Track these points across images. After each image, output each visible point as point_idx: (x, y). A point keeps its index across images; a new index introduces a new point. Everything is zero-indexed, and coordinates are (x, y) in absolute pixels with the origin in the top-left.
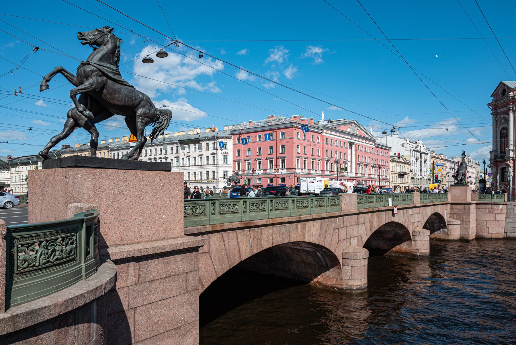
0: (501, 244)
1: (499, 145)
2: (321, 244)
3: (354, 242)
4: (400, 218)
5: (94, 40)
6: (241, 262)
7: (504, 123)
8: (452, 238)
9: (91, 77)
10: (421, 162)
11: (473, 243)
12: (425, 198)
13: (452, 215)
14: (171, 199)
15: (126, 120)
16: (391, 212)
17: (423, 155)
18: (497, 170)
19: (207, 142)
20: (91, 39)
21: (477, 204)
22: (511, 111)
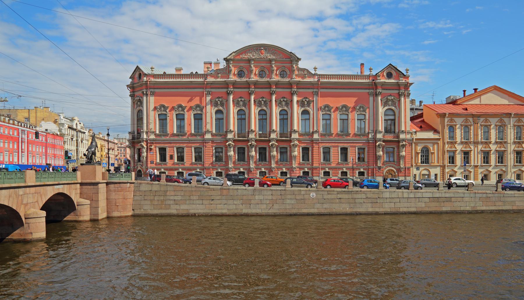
1: (136, 126)
7: (139, 106)
8: (81, 219)
10: (77, 140)
12: (44, 176)
13: (82, 195)
17: (80, 134)
18: (134, 151)
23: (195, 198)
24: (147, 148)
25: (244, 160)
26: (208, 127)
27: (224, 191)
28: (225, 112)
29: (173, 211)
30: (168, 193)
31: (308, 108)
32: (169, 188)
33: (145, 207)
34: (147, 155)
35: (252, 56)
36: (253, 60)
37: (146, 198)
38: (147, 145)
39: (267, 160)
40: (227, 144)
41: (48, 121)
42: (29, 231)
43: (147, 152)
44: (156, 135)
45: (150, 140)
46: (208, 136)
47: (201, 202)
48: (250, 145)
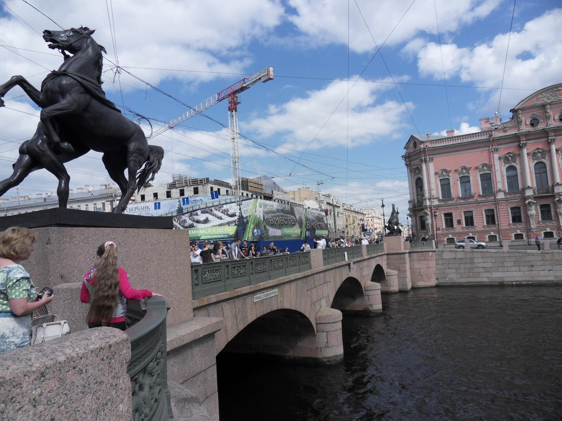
0: (434, 290)
2: (298, 310)
3: (323, 302)
4: (354, 273)
5: (69, 43)
6: (228, 343)
7: (418, 174)
9: (70, 94)
10: (334, 214)
11: (411, 293)
14: (177, 268)
15: (105, 160)
16: (348, 267)
18: (416, 219)
19: (104, 201)
20: (63, 41)
21: (409, 253)
22: (424, 163)
23: (509, 264)
24: (432, 215)
25: (550, 218)
26: (500, 186)
27: (547, 256)
28: (518, 167)
29: (484, 278)
30: (475, 260)
31: (513, 164)
32: (475, 255)
33: (451, 276)
34: (432, 221)
35: (546, 100)
36: (550, 104)
37: (450, 266)
38: (431, 212)
39: (553, 218)
40: (527, 202)
41: (310, 199)
42: (370, 303)
43: (432, 219)
44: (439, 200)
45: (435, 206)
46: (501, 196)
47: (517, 269)
48: (558, 200)
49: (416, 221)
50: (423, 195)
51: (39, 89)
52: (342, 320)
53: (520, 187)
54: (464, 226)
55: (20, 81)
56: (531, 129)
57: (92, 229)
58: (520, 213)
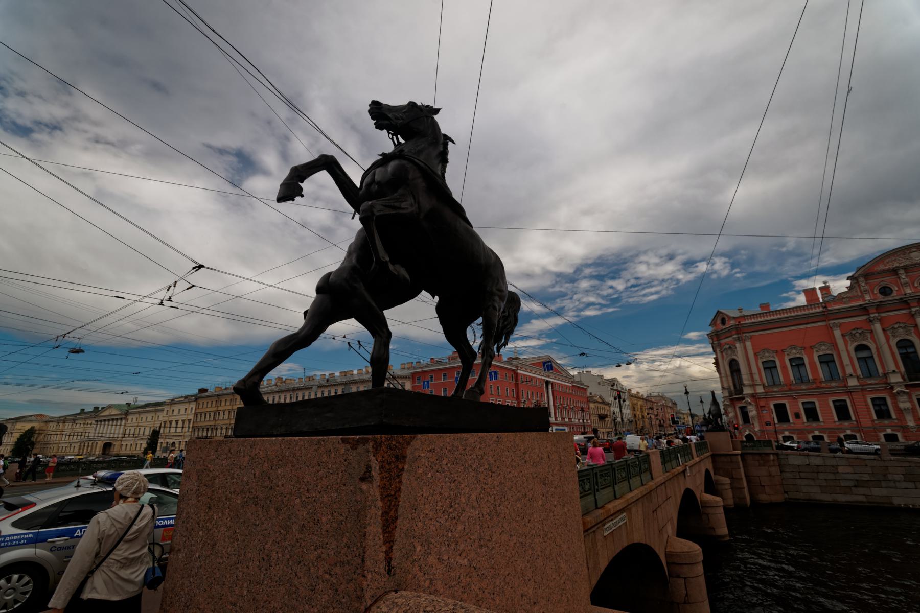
15: (439, 309)
20: (397, 118)
26: (849, 370)
28: (873, 346)
37: (802, 475)
47: (911, 485)
49: (736, 413)
50: (740, 379)
51: (358, 185)
52: (703, 561)
53: (880, 371)
54: (805, 420)
55: (329, 164)
56: (881, 298)
57: (448, 437)
58: (886, 404)
